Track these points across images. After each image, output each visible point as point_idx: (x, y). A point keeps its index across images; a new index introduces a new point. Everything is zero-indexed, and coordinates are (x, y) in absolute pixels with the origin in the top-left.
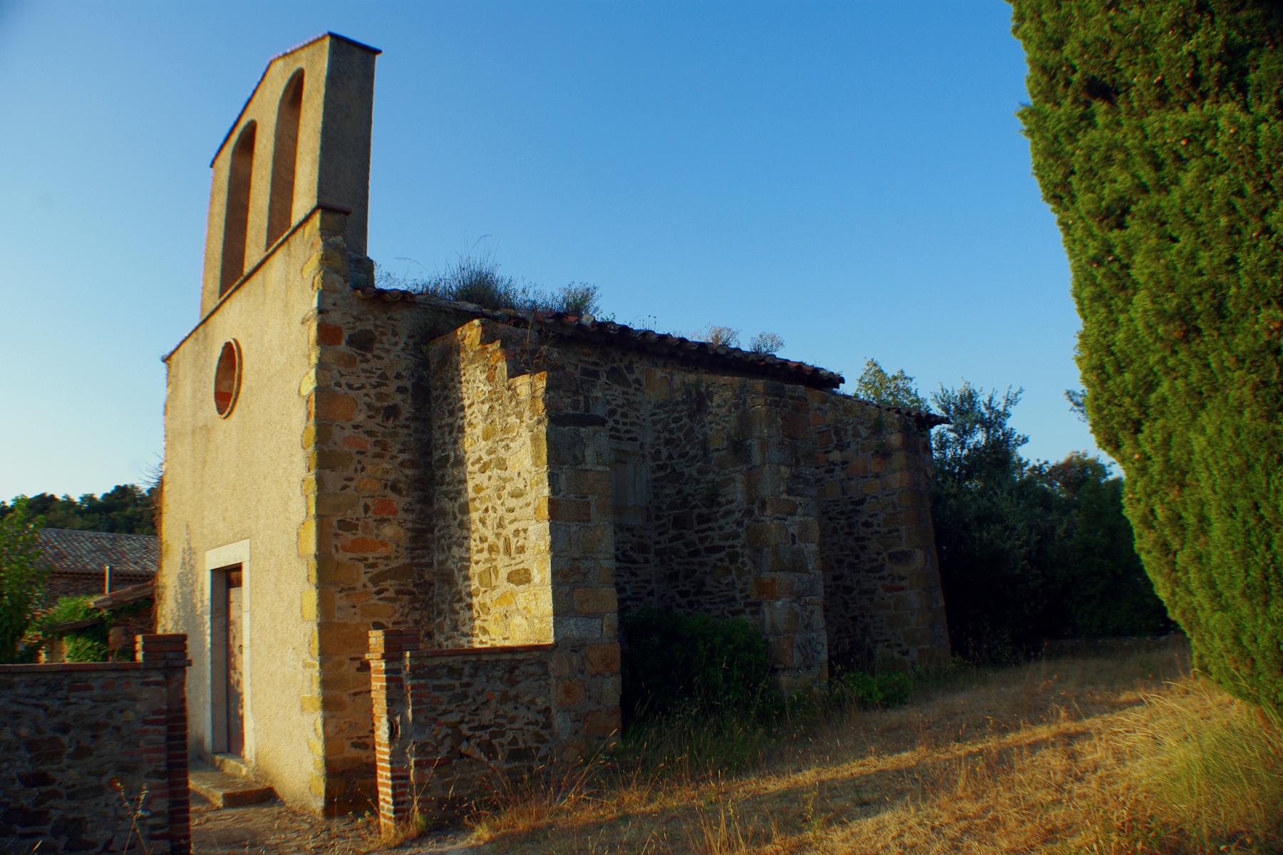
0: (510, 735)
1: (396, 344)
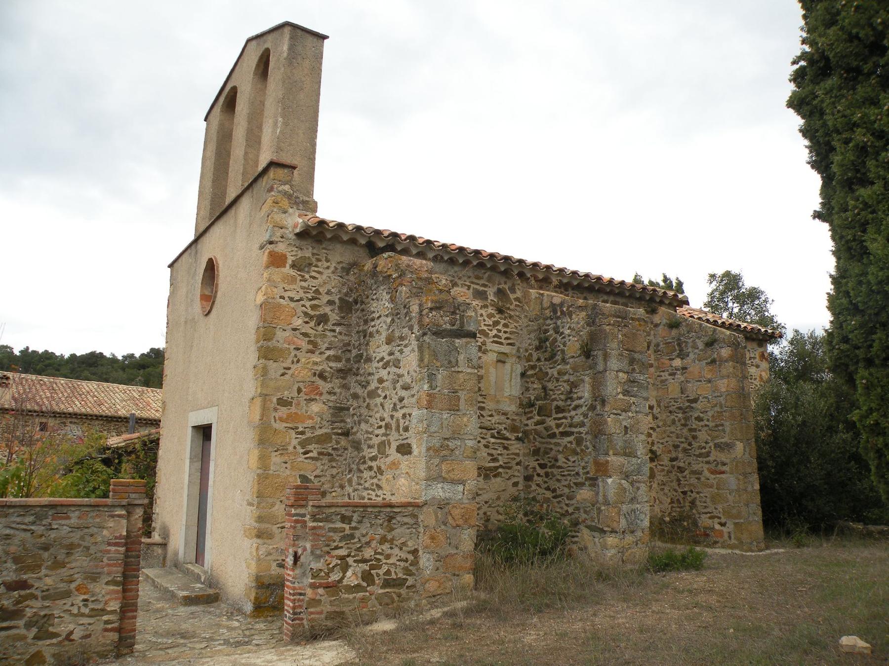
0: (385, 568)
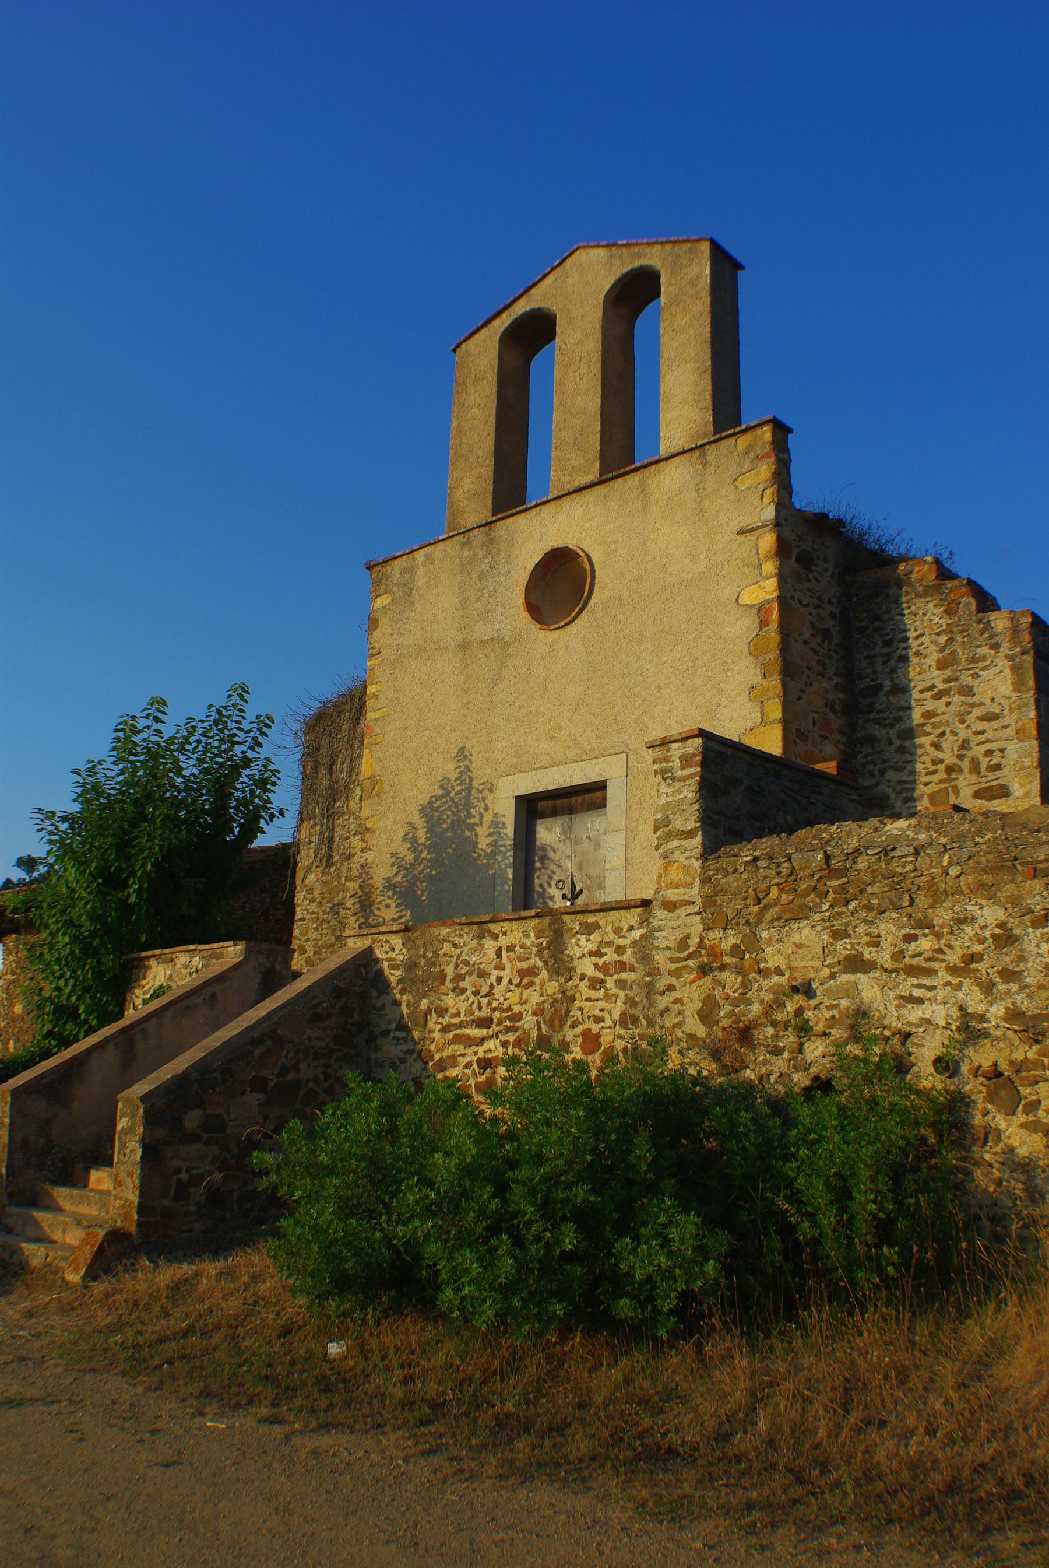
1: (826, 570)
